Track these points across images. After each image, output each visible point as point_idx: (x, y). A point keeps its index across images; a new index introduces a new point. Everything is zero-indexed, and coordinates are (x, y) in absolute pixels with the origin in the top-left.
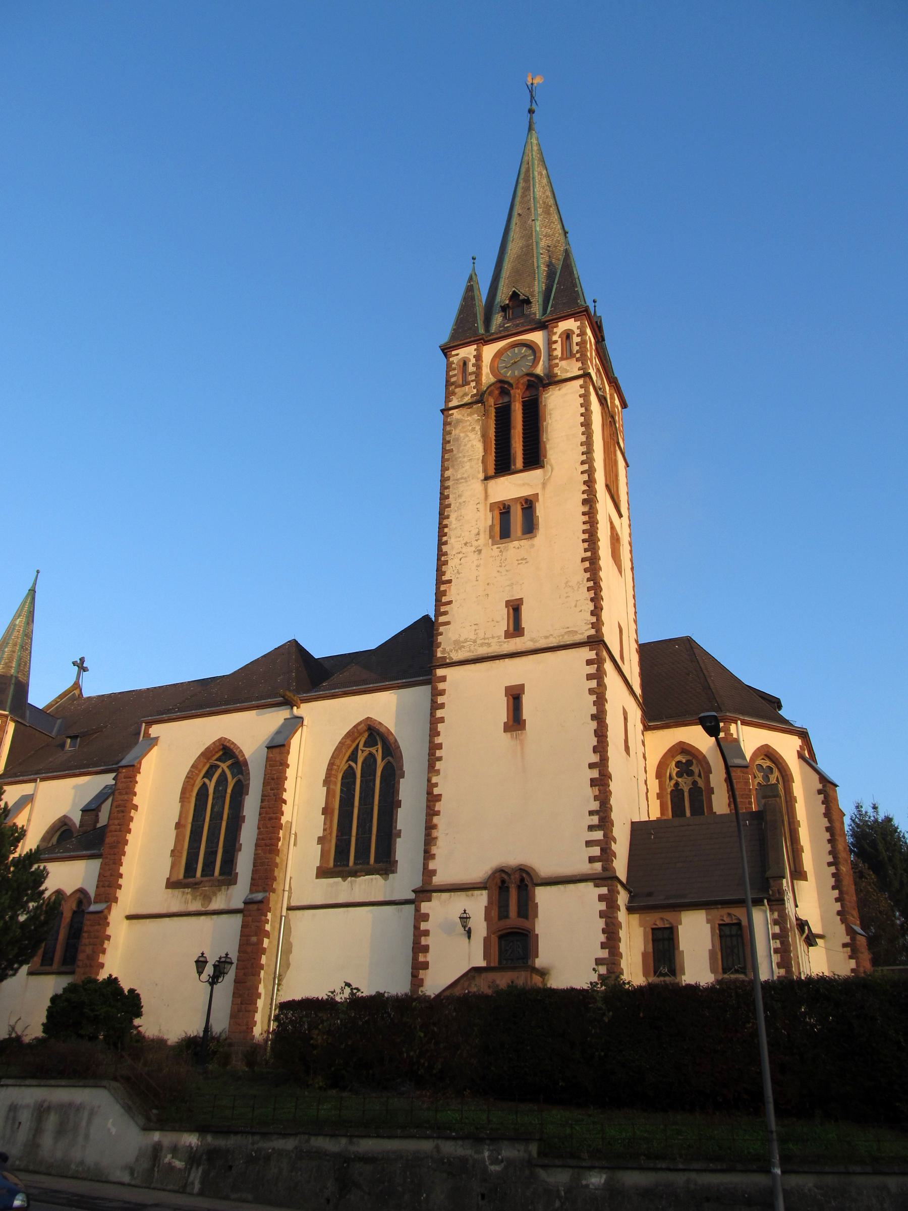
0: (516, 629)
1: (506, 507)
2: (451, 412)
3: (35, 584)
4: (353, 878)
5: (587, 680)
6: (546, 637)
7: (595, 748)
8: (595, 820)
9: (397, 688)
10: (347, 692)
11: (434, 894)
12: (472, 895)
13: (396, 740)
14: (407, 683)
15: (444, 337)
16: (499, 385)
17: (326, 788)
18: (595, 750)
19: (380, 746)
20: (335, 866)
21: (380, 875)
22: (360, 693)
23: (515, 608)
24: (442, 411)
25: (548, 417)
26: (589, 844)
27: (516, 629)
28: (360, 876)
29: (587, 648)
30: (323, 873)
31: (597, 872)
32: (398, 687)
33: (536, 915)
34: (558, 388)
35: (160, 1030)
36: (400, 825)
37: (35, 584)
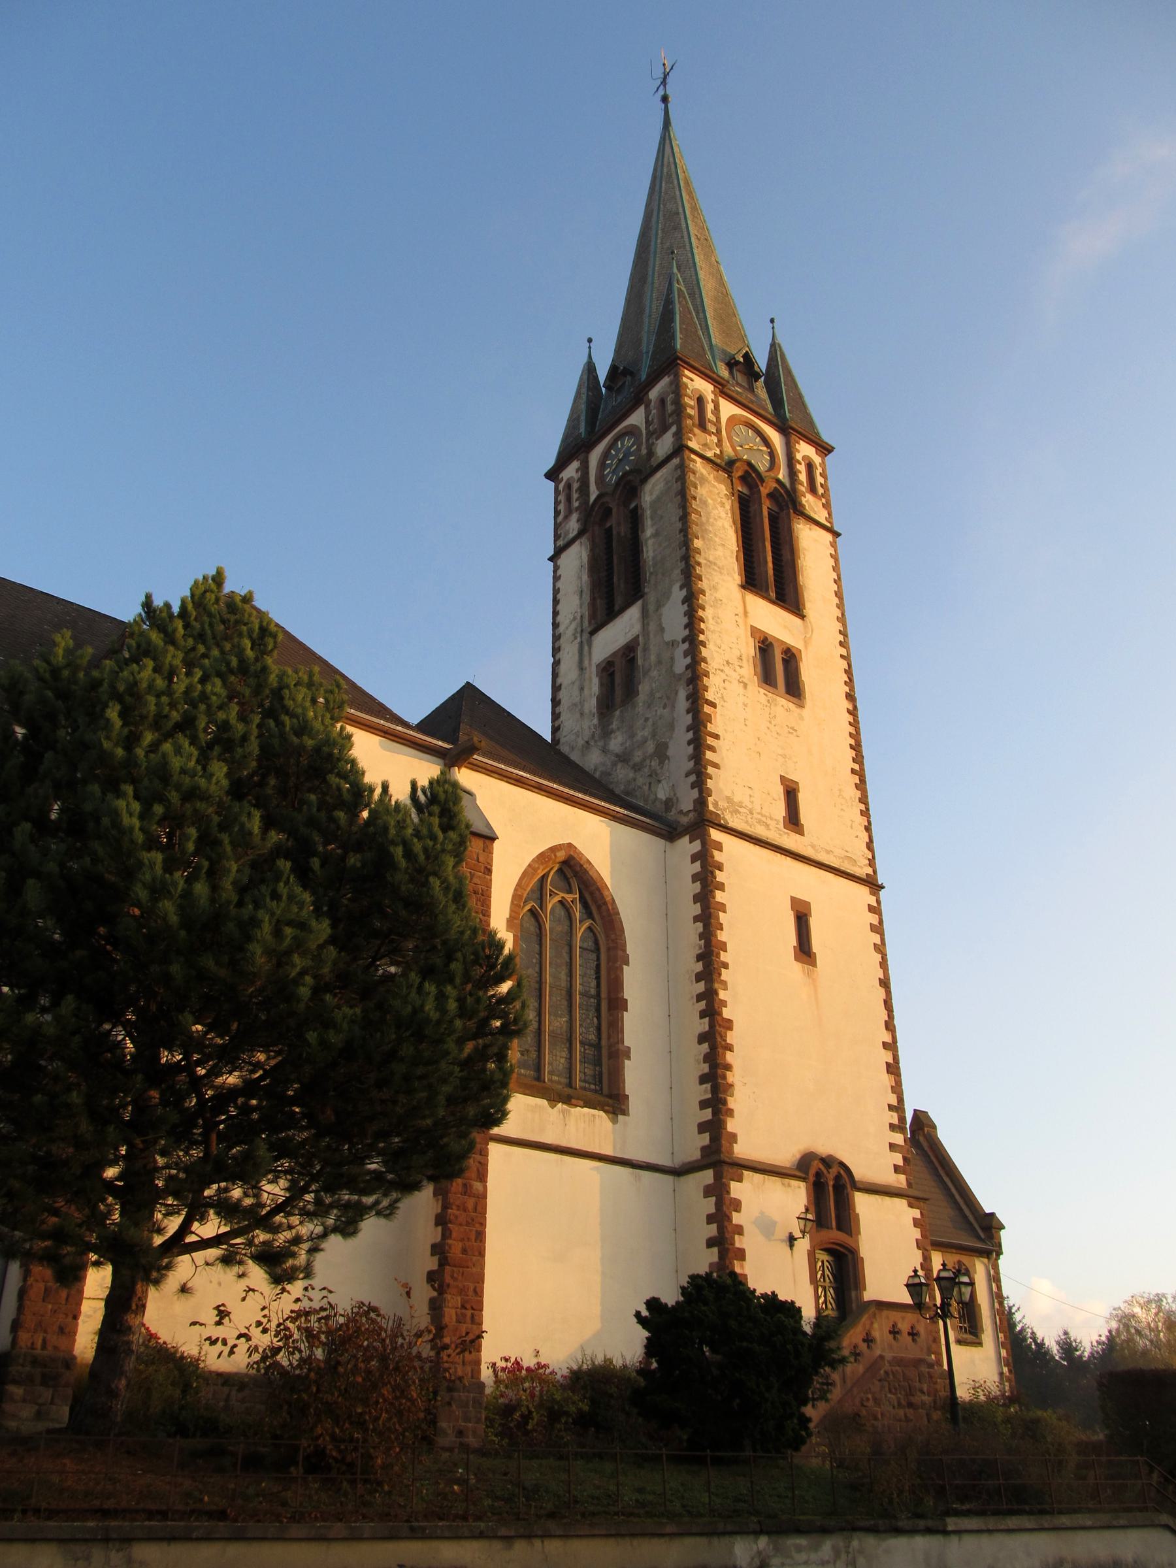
1: (767, 643)
3: (590, 356)
4: (565, 1106)
6: (828, 852)
9: (611, 818)
10: (543, 787)
11: (745, 1173)
12: (789, 1185)
13: (613, 899)
14: (653, 828)
15: (550, 462)
16: (746, 468)
21: (606, 1112)
22: (558, 798)
24: (550, 559)
25: (802, 556)
28: (576, 1106)
31: (900, 1186)
32: (614, 817)
33: (859, 1233)
34: (692, 489)
36: (629, 1039)
37: (590, 356)
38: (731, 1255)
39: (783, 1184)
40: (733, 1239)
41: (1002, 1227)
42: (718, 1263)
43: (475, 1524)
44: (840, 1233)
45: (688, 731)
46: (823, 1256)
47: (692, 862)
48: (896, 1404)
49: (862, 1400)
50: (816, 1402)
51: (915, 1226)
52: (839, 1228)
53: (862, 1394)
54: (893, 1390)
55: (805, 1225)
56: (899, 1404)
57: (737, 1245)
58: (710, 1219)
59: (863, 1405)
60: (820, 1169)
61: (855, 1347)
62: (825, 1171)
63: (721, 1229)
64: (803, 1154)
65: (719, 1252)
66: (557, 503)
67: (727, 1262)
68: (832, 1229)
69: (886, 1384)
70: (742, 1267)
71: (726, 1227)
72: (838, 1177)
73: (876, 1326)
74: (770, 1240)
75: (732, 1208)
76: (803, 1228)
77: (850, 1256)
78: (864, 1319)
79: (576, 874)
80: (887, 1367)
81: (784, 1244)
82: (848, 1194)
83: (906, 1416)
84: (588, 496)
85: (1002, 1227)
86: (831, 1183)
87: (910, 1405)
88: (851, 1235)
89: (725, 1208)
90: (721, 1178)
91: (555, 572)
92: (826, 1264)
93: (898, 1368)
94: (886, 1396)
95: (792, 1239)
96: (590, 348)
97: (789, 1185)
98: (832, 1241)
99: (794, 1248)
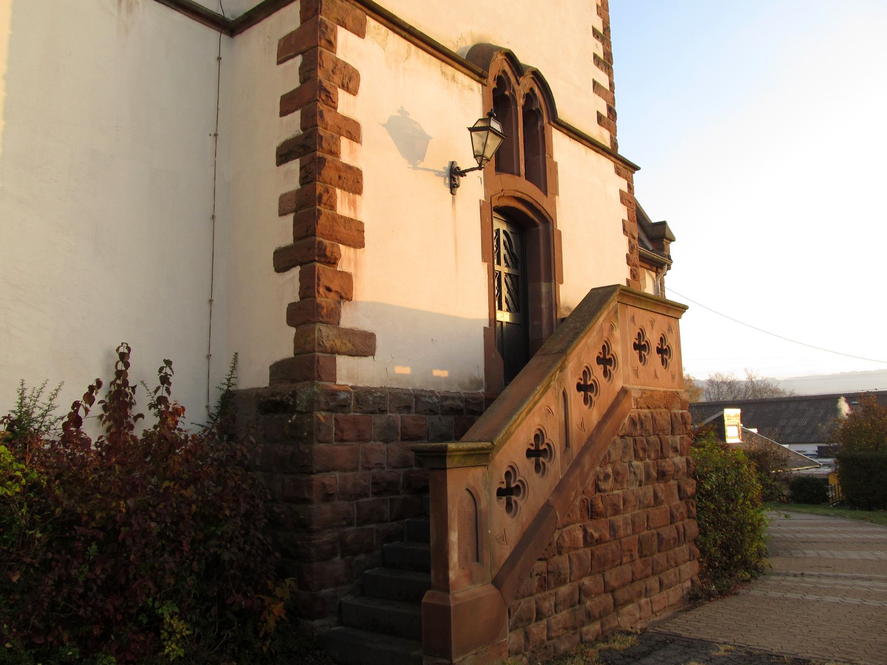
12: (453, 79)
33: (556, 193)
38: (328, 173)
39: (443, 73)
40: (337, 144)
41: (672, 239)
42: (298, 191)
44: (529, 184)
46: (500, 225)
47: (283, 113)
48: (643, 477)
49: (598, 478)
50: (514, 498)
51: (622, 202)
52: (528, 177)
53: (598, 468)
54: (641, 454)
55: (485, 145)
56: (648, 476)
57: (345, 157)
58: (288, 104)
59: (598, 489)
60: (504, 72)
61: (586, 373)
62: (513, 79)
63: (310, 123)
64: (476, 42)
65: (302, 168)
67: (319, 188)
68: (519, 175)
69: (630, 441)
70: (353, 205)
71: (322, 116)
72: (530, 97)
73: (617, 333)
74: (415, 168)
75: (337, 79)
76: (478, 147)
77: (541, 227)
78: (601, 319)
80: (633, 412)
81: (441, 180)
82: (543, 128)
83: (656, 496)
85: (672, 239)
86: (521, 102)
87: (662, 475)
88: (545, 192)
89: (320, 75)
90: (317, 12)
92: (502, 237)
93: (647, 411)
94: (630, 465)
95: (455, 174)
97: (453, 79)
98: (519, 195)
99: (458, 191)
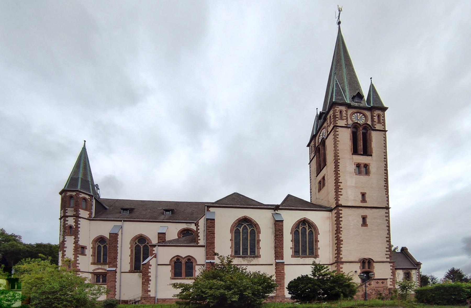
0: (364, 200)
2: (338, 128)
5: (159, 233)
7: (130, 248)
8: (388, 250)
17: (291, 235)
18: (388, 234)
19: (307, 225)
20: (97, 262)
23: (363, 195)
24: (309, 164)
26: (386, 254)
27: (364, 200)
29: (386, 209)
30: (292, 256)
35: (365, 293)
43: (361, 134)
45: (335, 218)
66: (310, 151)
79: (307, 222)
82: (372, 263)
84: (316, 145)
91: (310, 166)
96: (317, 111)
